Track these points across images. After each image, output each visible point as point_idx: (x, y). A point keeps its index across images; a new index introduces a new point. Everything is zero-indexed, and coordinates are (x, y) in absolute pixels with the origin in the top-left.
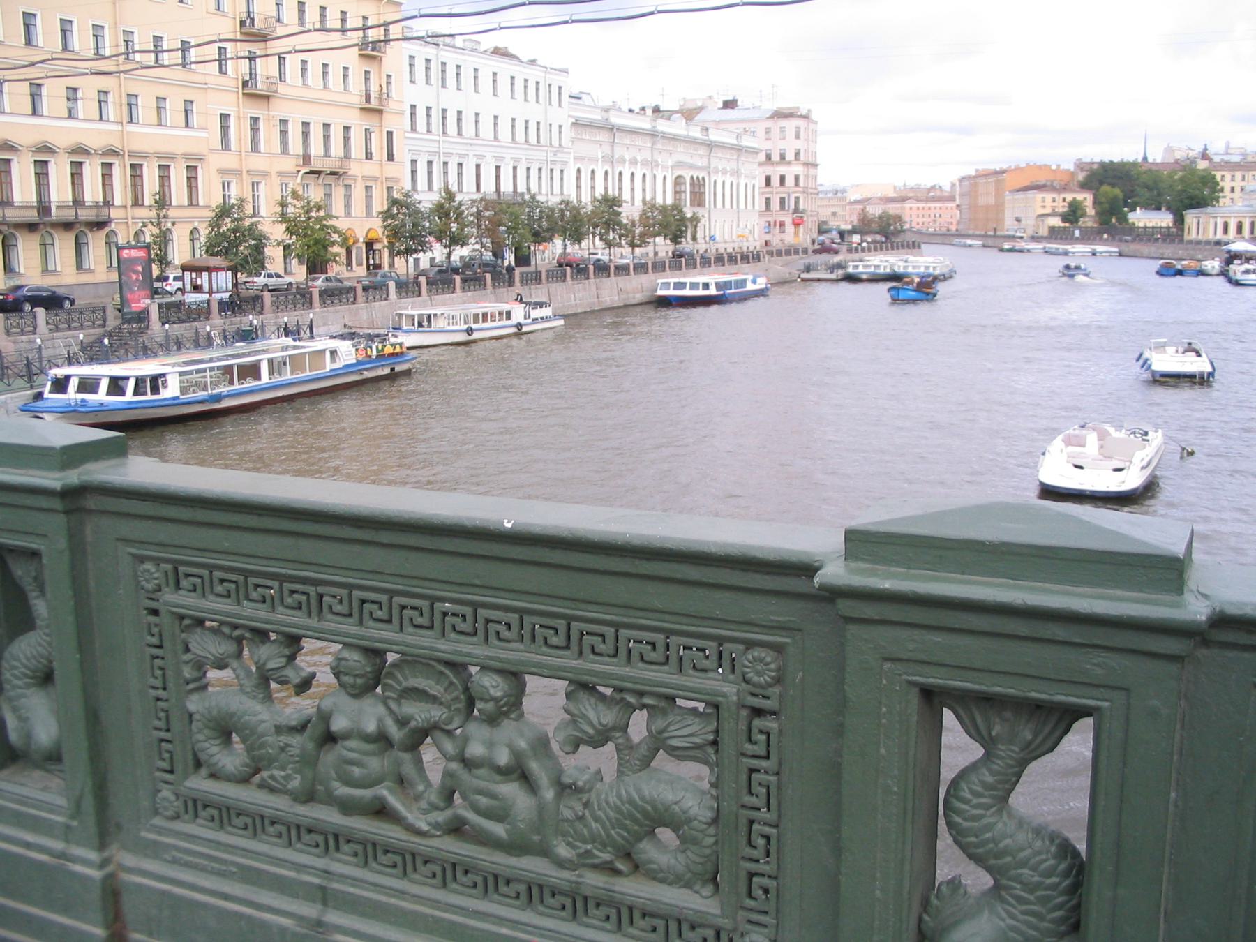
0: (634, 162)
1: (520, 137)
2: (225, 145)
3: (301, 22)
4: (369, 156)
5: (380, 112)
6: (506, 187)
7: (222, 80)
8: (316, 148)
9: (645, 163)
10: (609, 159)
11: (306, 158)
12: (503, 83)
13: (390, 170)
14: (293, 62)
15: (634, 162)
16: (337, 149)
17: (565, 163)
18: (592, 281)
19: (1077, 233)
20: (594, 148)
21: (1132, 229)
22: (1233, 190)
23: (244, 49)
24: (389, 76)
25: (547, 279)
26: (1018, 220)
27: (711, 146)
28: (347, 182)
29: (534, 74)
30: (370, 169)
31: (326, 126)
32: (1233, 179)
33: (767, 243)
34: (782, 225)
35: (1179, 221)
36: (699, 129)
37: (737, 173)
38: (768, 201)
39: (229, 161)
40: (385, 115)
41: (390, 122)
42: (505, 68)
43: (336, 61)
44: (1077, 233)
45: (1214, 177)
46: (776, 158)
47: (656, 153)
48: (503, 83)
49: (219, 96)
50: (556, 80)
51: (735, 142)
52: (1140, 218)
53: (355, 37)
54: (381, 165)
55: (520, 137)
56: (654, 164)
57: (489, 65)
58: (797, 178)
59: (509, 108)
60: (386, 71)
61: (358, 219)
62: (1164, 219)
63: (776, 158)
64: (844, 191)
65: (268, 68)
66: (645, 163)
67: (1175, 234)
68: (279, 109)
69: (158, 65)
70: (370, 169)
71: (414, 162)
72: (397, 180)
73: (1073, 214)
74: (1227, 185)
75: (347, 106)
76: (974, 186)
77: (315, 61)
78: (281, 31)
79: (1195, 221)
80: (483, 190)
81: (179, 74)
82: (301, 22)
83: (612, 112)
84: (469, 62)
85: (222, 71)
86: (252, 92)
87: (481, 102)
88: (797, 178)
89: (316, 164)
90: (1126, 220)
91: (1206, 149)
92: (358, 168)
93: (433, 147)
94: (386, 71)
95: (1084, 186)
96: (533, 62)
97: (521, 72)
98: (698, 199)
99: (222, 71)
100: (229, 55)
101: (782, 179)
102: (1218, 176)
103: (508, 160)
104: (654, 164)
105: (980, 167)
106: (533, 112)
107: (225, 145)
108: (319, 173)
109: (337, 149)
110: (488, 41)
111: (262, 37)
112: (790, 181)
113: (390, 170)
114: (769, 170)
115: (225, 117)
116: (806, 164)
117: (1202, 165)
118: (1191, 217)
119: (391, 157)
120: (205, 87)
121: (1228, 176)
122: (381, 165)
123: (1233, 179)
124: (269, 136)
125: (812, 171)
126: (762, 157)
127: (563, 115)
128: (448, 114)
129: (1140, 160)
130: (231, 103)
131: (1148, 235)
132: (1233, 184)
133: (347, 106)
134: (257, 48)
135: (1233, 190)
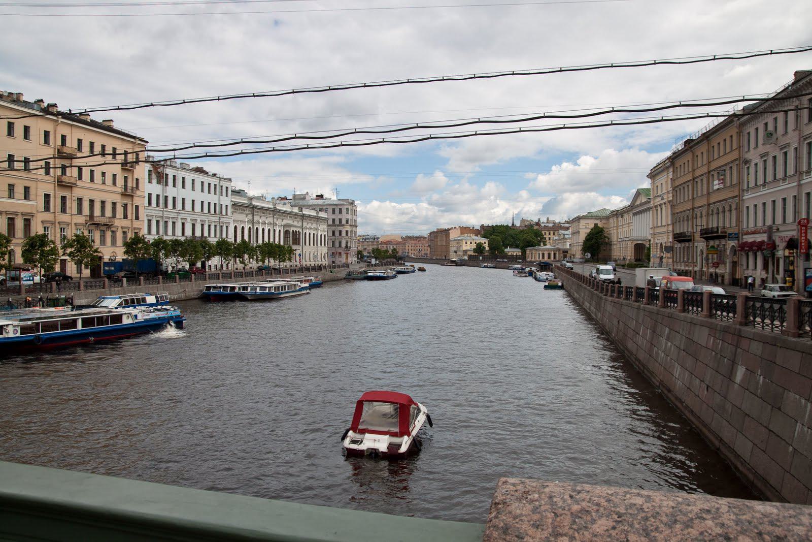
0: (264, 223)
1: (206, 210)
2: (47, 208)
3: (92, 172)
4: (125, 217)
5: (132, 196)
6: (198, 233)
7: (47, 177)
8: (97, 212)
9: (270, 224)
10: (253, 222)
11: (91, 216)
12: (198, 186)
13: (136, 224)
14: (86, 173)
15: (264, 223)
16: (108, 213)
17: (229, 223)
18: (244, 278)
19: (481, 258)
20: (243, 218)
21: (505, 256)
22: (550, 239)
23: (59, 162)
24: (137, 180)
25: (209, 278)
26: (455, 252)
27: (303, 217)
28: (112, 229)
29: (214, 181)
30: (126, 223)
31: (103, 203)
32: (550, 234)
33: (333, 262)
34: (340, 253)
35: (524, 252)
36: (297, 208)
37: (317, 229)
38: (333, 242)
39: (48, 217)
40: (134, 197)
41: (137, 201)
42: (199, 178)
43: (110, 170)
44: (481, 258)
45: (541, 232)
46: (337, 222)
47: (275, 220)
48: (198, 186)
49: (44, 185)
50: (225, 184)
51: (315, 215)
52: (509, 251)
53: (120, 158)
54: (132, 222)
55: (206, 210)
56: (274, 224)
57: (189, 176)
58: (347, 232)
59: (200, 196)
60: (136, 176)
61: (113, 251)
62: (517, 252)
63: (337, 222)
64: (378, 238)
65: (72, 173)
66: (270, 224)
67: (524, 257)
68: (77, 193)
69: (11, 168)
70: (126, 223)
71: (149, 221)
72: (140, 229)
73: (479, 248)
74: (547, 236)
75: (115, 192)
76: (430, 236)
77: (98, 171)
78: (79, 155)
79: (530, 253)
80: (186, 234)
81: (23, 174)
82: (92, 172)
83: (253, 200)
84: (181, 174)
85: (47, 173)
86: (61, 184)
87: (187, 194)
88: (347, 232)
89: (96, 220)
90: (504, 251)
91: (539, 220)
92: (119, 222)
93: (160, 214)
94: (136, 176)
95: (484, 236)
96: (214, 175)
97: (207, 180)
98: (296, 241)
99: (47, 173)
100: (51, 166)
101: (340, 232)
102: (543, 232)
103: (199, 221)
104: (274, 224)
105: (439, 228)
106: (213, 198)
107: (47, 208)
108: (98, 224)
109: (108, 213)
110: (194, 164)
111: (71, 157)
112: (344, 234)
113: (136, 224)
114: (333, 228)
115: (47, 196)
116: (351, 226)
117: (536, 227)
118: (528, 252)
119: (137, 218)
120: (37, 180)
121: (547, 233)
122: (132, 222)
123: (550, 234)
124: (72, 206)
125: (354, 229)
126: (330, 222)
127: (226, 201)
128: (186, 181)
129: (510, 225)
130: (49, 189)
131: (513, 259)
132: (550, 236)
133: (115, 192)
134: (66, 162)
135: (550, 239)
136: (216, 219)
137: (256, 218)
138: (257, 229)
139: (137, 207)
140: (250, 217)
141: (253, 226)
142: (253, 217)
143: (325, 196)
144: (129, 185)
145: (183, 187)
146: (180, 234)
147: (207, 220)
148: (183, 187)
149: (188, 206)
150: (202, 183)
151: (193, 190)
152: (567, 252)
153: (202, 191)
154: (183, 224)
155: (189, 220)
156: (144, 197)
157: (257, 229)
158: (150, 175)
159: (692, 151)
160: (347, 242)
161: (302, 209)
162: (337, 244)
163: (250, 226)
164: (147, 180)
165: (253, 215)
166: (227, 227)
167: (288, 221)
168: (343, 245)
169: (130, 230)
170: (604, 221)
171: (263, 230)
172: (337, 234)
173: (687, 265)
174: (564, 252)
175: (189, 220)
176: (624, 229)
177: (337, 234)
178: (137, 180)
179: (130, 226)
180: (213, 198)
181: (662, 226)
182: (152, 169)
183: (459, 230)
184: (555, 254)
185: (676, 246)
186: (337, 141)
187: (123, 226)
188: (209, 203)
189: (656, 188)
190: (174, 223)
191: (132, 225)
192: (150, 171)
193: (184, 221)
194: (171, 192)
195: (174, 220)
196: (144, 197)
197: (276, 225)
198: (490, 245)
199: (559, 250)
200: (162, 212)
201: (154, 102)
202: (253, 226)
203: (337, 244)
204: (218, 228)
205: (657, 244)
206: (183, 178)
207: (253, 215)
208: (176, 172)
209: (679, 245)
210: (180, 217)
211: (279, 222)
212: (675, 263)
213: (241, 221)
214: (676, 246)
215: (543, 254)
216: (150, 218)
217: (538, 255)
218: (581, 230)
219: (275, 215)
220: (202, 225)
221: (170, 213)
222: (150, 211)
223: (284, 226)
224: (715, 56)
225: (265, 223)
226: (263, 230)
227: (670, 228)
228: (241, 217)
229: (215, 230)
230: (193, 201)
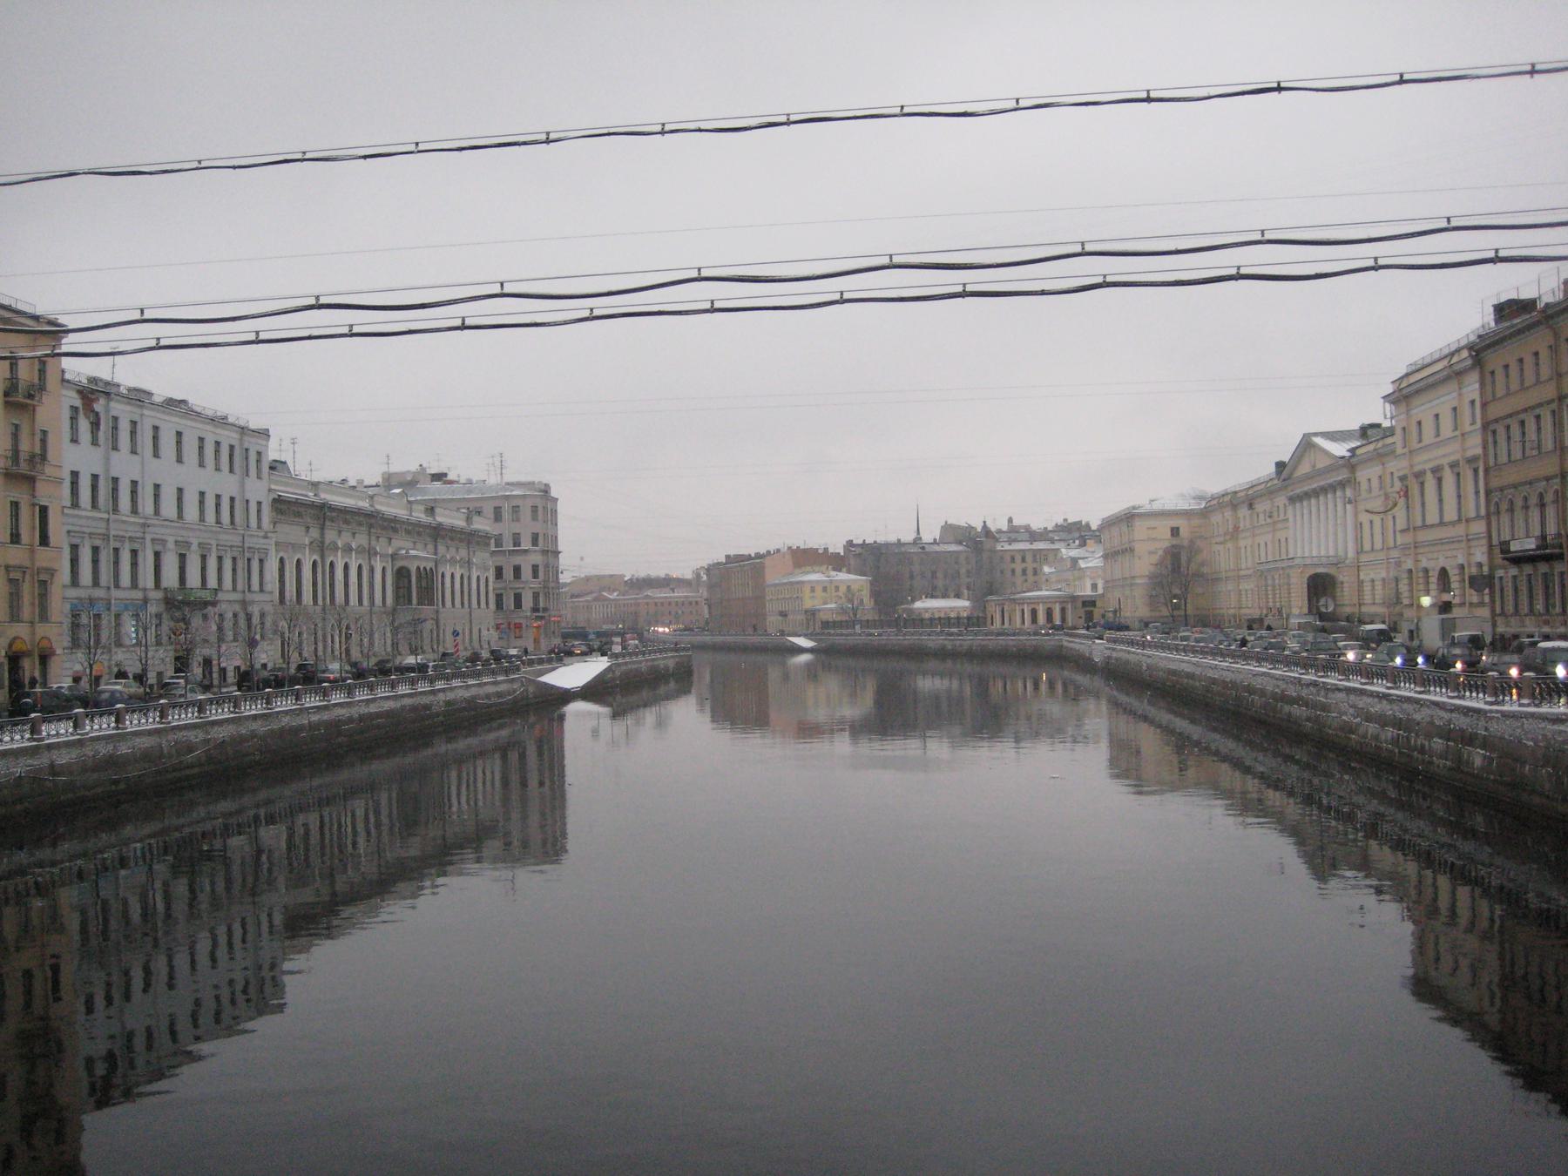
0: (348, 549)
5: (31, 480)
26: (784, 614)
40: (39, 485)
41: (44, 494)
46: (508, 545)
56: (371, 553)
58: (535, 569)
71: (75, 548)
101: (517, 570)
103: (194, 547)
104: (371, 553)
105: (732, 552)
106: (226, 484)
112: (526, 573)
113: (43, 557)
116: (545, 552)
119: (44, 540)
127: (258, 490)
128: (185, 439)
136: (236, 541)
137: (330, 535)
138: (332, 564)
139: (44, 511)
140: (314, 533)
141: (323, 557)
142: (322, 535)
143: (451, 477)
144: (25, 446)
145: (156, 455)
146: (150, 584)
147: (214, 543)
148: (156, 455)
149: (168, 508)
150: (201, 440)
151: (179, 460)
152: (1093, 603)
153: (201, 464)
154: (157, 555)
155: (170, 545)
156: (59, 481)
157: (332, 564)
158: (73, 419)
159: (1550, 327)
160: (536, 596)
161: (432, 509)
162: (509, 602)
163: (315, 557)
164: (67, 435)
165: (322, 528)
166: (261, 561)
167: (402, 544)
168: (528, 602)
169: (28, 577)
170: (1196, 522)
171: (346, 567)
172: (508, 574)
173: (1547, 623)
174: (1084, 604)
175: (170, 545)
176: (1257, 540)
177: (508, 574)
178: (44, 433)
179: (27, 563)
180: (226, 484)
181: (1442, 523)
182: (78, 403)
183: (788, 557)
184: (1063, 610)
185: (1500, 573)
186: (830, 288)
187: (12, 563)
188: (218, 497)
189: (1414, 429)
190: (134, 553)
191: (32, 559)
192: (74, 409)
193: (159, 548)
194: (125, 466)
195: (136, 546)
196: (59, 481)
197: (376, 553)
198: (875, 594)
199: (1074, 598)
200: (103, 525)
201: (554, 126)
202: (323, 557)
203: (509, 602)
204: (241, 565)
205: (1426, 571)
206: (156, 428)
207: (322, 528)
208: (138, 411)
209: (1514, 571)
210: (148, 537)
211: (381, 546)
212: (1499, 620)
213: (293, 545)
214: (1500, 573)
215: (1034, 613)
216: (75, 541)
217: (1018, 614)
218: (1138, 547)
219: (371, 526)
220: (204, 558)
221: (125, 522)
222: (75, 520)
223: (394, 557)
224: (317, 298)
225: (351, 549)
226: (346, 567)
227: (1479, 527)
228: (293, 532)
229: (220, 570)
230: (180, 490)
